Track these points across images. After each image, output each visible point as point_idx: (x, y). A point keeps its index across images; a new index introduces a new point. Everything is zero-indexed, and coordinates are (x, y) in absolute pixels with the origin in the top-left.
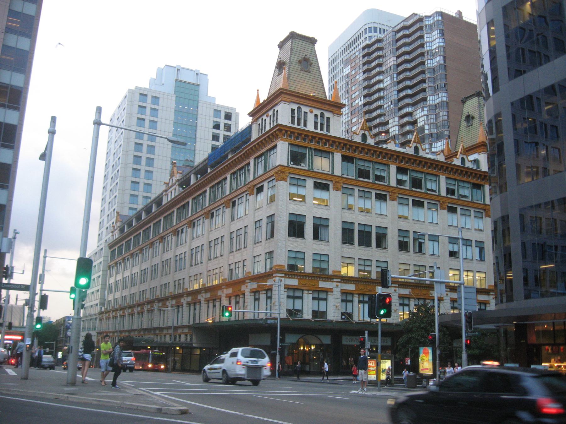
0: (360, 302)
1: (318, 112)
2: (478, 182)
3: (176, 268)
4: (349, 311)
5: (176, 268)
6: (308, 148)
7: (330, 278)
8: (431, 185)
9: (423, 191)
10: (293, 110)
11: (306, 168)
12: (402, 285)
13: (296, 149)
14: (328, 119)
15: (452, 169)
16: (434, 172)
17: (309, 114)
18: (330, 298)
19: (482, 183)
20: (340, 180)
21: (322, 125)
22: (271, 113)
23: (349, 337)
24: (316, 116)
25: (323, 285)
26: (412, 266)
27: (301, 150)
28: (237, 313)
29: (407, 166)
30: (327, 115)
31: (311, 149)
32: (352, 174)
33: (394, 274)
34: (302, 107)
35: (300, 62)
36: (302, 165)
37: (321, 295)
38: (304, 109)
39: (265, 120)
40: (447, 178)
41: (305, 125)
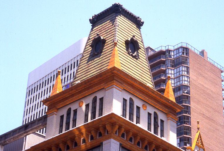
1: (152, 111)
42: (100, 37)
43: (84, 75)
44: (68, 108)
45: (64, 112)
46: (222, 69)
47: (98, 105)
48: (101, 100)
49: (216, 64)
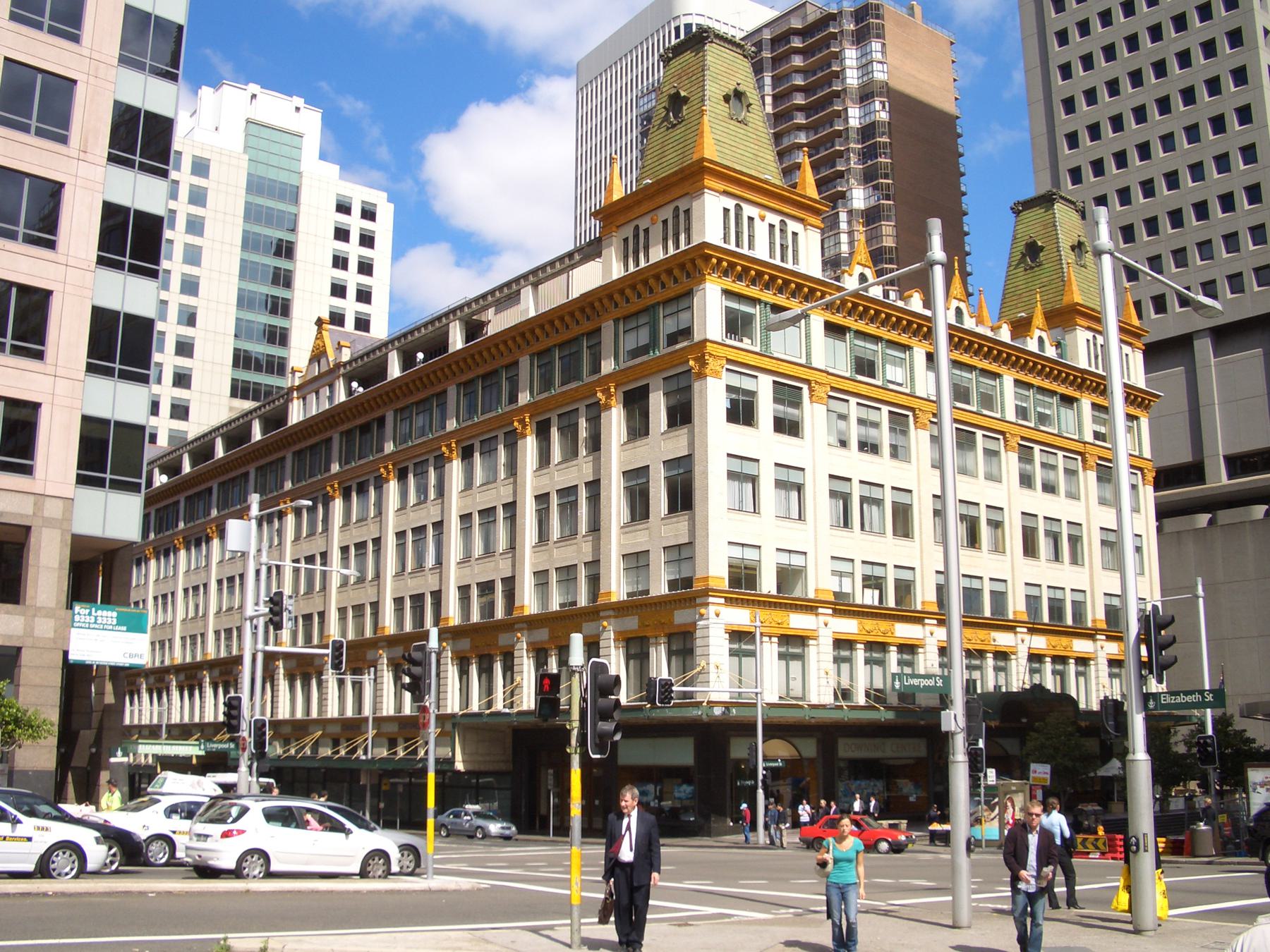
0: (867, 662)
1: (775, 219)
2: (1070, 392)
3: (377, 552)
4: (845, 683)
5: (377, 552)
6: (760, 301)
7: (809, 607)
8: (894, 373)
9: (879, 383)
10: (726, 211)
11: (757, 349)
12: (842, 606)
13: (735, 305)
14: (795, 234)
15: (799, 287)
16: (904, 339)
17: (757, 221)
18: (812, 651)
19: (1076, 394)
20: (822, 378)
21: (784, 248)
22: (667, 213)
23: (850, 741)
24: (772, 226)
25: (798, 622)
26: (858, 564)
27: (745, 308)
28: (315, 641)
29: (849, 322)
30: (793, 226)
31: (766, 304)
32: (844, 367)
33: (820, 582)
34: (788, 221)
35: (727, 99)
36: (746, 340)
37: (794, 644)
38: (748, 210)
39: (646, 231)
40: (1018, 383)
41: (751, 246)
42: (678, 93)
45: (628, 231)
47: (683, 221)
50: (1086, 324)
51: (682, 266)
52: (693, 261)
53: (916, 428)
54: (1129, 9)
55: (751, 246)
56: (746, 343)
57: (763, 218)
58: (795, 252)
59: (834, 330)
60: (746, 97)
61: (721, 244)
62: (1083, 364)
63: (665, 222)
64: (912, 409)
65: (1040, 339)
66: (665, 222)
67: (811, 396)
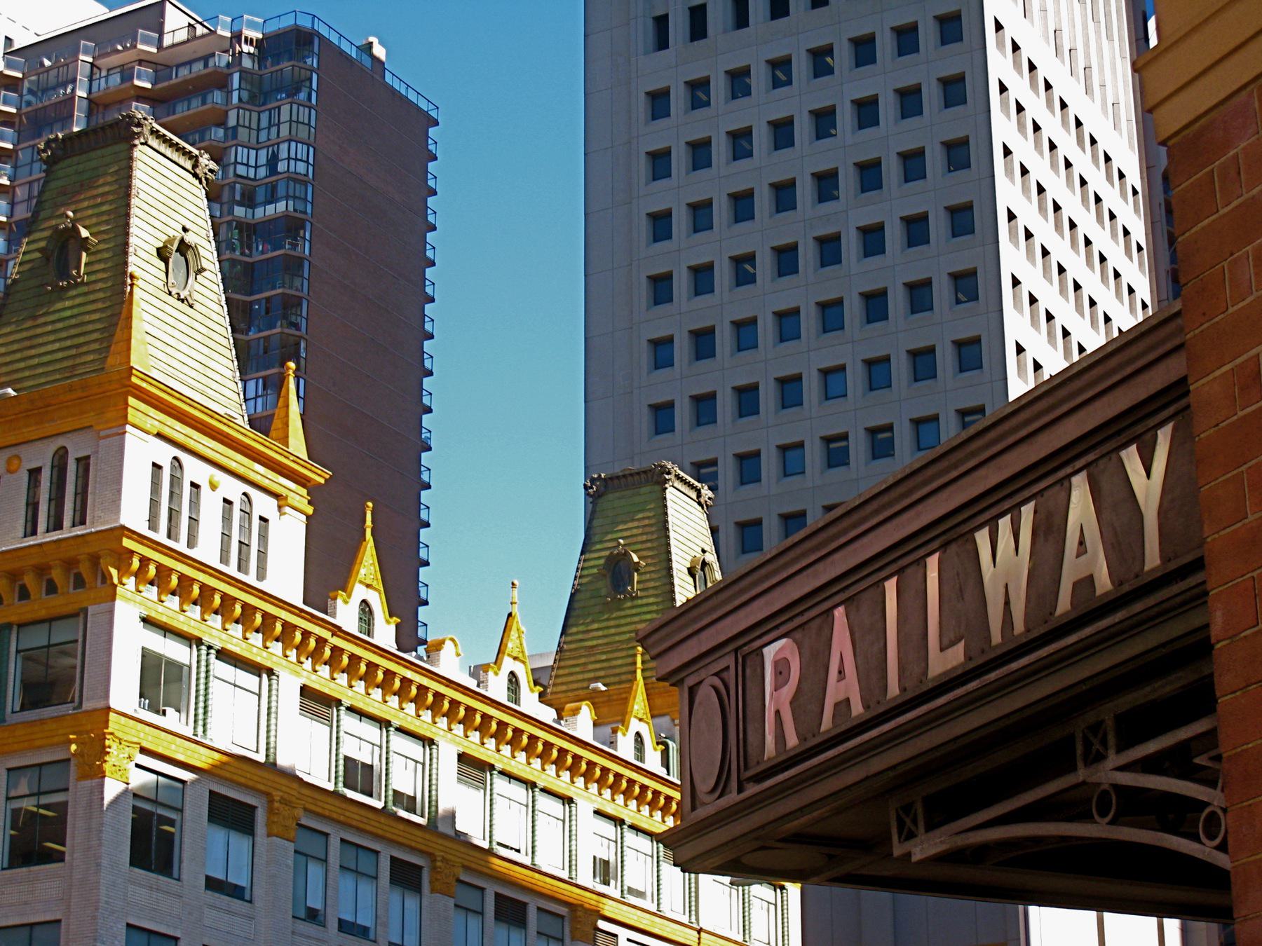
1: (235, 490)
17: (205, 489)
21: (173, 514)
38: (195, 470)
41: (191, 543)
43: (18, 356)
44: (52, 447)
45: (41, 456)
46: (433, 114)
48: (84, 462)
49: (412, 97)
50: (156, 427)
51: (70, 564)
52: (95, 560)
53: (433, 891)
54: (779, 7)
55: (191, 543)
56: (172, 719)
57: (213, 487)
58: (262, 555)
59: (316, 701)
60: (197, 255)
61: (214, 562)
62: (207, 551)
63: (35, 473)
64: (431, 856)
65: (513, 678)
66: (35, 473)
67: (269, 824)
